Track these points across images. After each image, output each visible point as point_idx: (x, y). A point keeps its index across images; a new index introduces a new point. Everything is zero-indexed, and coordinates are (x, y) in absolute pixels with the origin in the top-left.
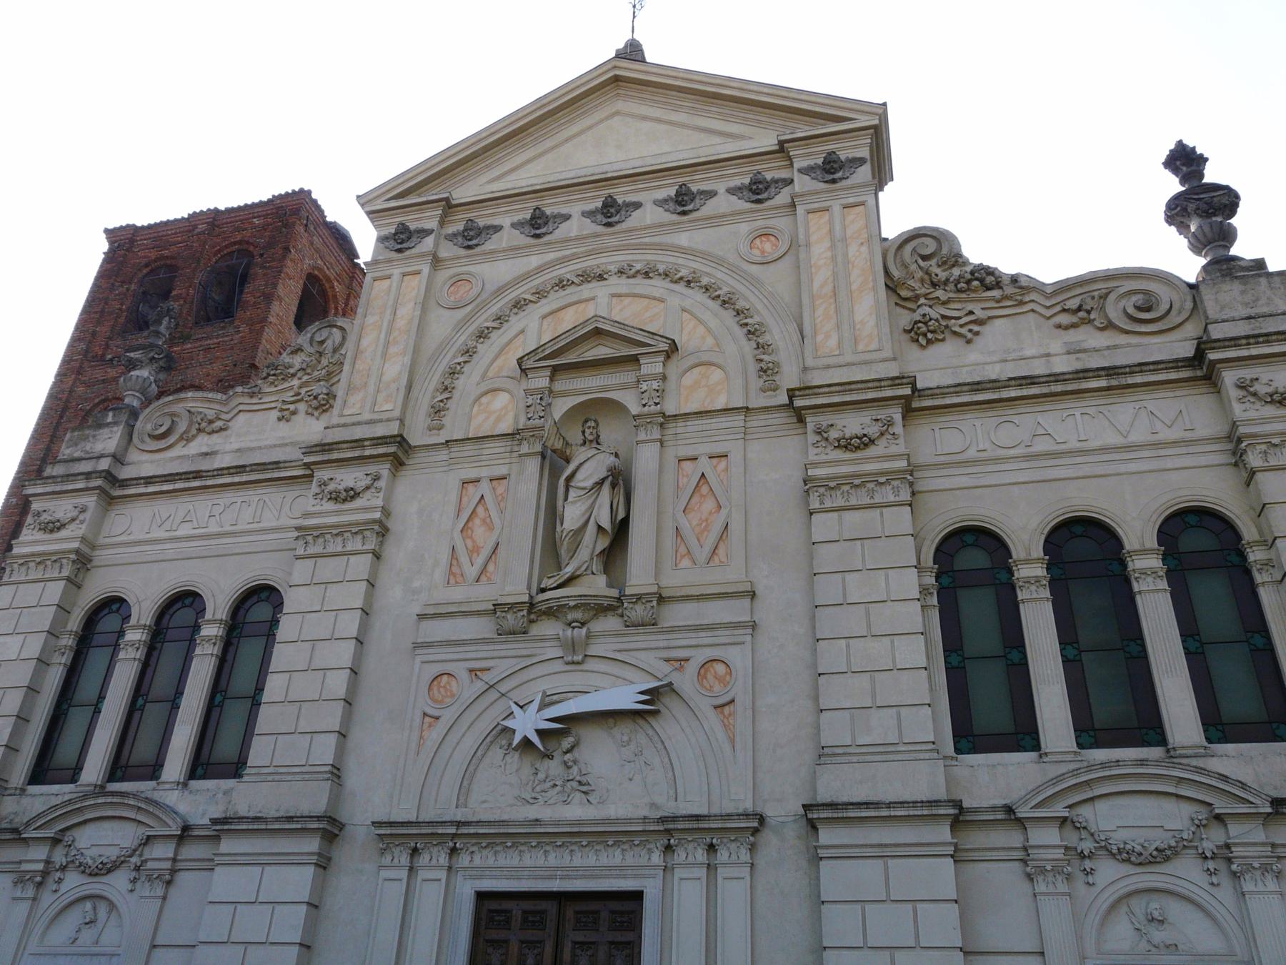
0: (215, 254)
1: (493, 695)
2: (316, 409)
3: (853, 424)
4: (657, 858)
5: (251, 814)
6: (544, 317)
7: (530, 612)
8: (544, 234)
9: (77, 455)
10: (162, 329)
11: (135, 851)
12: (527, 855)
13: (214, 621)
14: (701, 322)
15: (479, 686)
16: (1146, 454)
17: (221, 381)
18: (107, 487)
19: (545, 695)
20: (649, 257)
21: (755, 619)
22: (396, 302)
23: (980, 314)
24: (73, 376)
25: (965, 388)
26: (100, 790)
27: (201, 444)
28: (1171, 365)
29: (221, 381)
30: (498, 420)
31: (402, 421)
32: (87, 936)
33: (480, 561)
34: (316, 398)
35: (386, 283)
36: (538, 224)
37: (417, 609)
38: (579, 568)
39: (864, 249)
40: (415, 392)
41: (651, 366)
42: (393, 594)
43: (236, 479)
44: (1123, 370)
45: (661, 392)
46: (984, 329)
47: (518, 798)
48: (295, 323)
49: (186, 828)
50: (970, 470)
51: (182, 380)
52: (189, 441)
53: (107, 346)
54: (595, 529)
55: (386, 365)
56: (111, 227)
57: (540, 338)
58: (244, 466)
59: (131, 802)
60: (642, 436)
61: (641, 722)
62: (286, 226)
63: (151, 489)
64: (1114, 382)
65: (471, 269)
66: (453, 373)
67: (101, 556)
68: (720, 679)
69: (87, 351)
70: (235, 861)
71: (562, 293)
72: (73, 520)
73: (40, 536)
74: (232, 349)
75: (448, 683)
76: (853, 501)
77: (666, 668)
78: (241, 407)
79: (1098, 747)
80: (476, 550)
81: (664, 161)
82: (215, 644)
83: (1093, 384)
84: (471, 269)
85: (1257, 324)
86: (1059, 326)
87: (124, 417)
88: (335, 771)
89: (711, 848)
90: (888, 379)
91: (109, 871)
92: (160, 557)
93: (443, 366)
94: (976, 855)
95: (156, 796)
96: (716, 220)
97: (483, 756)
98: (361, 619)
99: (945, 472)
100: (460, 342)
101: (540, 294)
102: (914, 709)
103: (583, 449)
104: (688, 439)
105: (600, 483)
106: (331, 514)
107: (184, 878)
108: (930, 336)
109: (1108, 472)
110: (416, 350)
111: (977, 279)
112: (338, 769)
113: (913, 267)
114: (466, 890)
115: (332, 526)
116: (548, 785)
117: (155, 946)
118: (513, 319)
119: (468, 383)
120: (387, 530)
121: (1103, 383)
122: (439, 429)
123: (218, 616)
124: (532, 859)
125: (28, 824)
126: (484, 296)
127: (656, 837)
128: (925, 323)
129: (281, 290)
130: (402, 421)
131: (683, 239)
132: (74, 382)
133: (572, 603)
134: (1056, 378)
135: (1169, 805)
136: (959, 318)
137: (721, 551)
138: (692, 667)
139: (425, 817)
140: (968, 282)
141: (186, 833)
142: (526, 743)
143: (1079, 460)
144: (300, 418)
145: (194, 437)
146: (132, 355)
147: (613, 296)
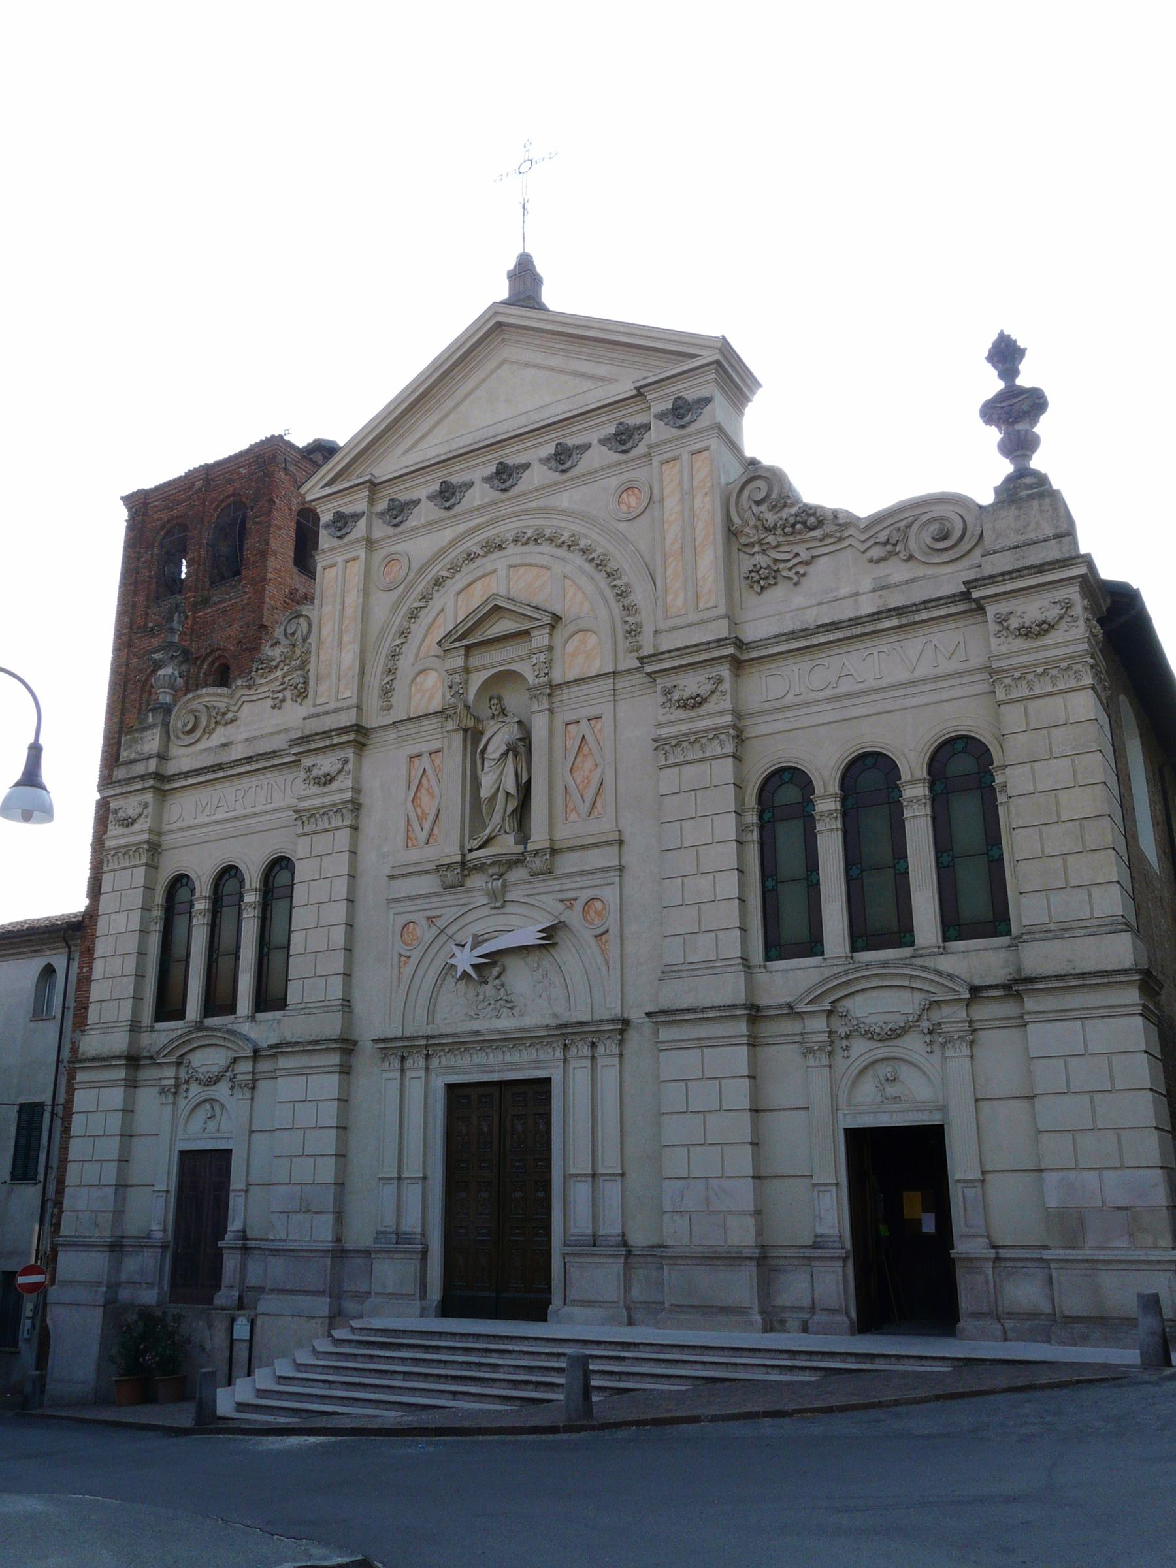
0: (215, 510)
1: (443, 938)
2: (298, 696)
3: (692, 684)
4: (559, 1054)
5: (294, 1040)
6: (459, 593)
7: (463, 869)
8: (454, 505)
9: (133, 756)
10: (175, 625)
11: (228, 1068)
12: (475, 1056)
13: (251, 890)
14: (579, 588)
15: (434, 931)
16: (928, 687)
17: (240, 642)
18: (158, 785)
19: (475, 936)
20: (537, 522)
21: (623, 863)
22: (343, 591)
23: (805, 556)
24: (126, 650)
25: (783, 638)
26: (200, 1026)
27: (220, 735)
28: (950, 600)
29: (240, 642)
30: (431, 697)
31: (359, 707)
32: (211, 1125)
33: (427, 825)
34: (296, 688)
35: (334, 571)
36: (447, 494)
37: (387, 871)
38: (493, 831)
39: (707, 499)
40: (367, 677)
41: (540, 639)
42: (369, 859)
43: (248, 768)
44: (910, 609)
45: (549, 663)
46: (811, 569)
47: (466, 1014)
48: (296, 564)
49: (256, 1051)
50: (788, 714)
51: (210, 645)
52: (211, 733)
53: (147, 614)
54: (504, 794)
55: (343, 655)
56: (125, 494)
57: (456, 615)
58: (250, 757)
59: (219, 1034)
60: (535, 707)
61: (544, 951)
62: (266, 475)
63: (191, 781)
64: (904, 621)
65: (399, 548)
66: (394, 655)
67: (168, 840)
68: (599, 914)
69: (132, 623)
70: (288, 1073)
71: (472, 566)
72: (140, 815)
73: (121, 831)
74: (243, 609)
75: (414, 929)
76: (690, 757)
77: (561, 907)
78: (244, 699)
79: (868, 950)
80: (421, 819)
81: (547, 415)
82: (255, 908)
83: (887, 624)
84: (399, 548)
85: (1022, 554)
86: (871, 561)
87: (160, 717)
88: (346, 1003)
89: (593, 1045)
90: (714, 641)
91: (215, 1083)
92: (207, 839)
93: (385, 651)
94: (770, 1041)
95: (236, 1027)
96: (591, 476)
97: (441, 984)
98: (348, 884)
99: (768, 718)
100: (397, 623)
101: (455, 569)
102: (728, 931)
103: (492, 722)
104: (573, 705)
105: (506, 754)
106: (318, 798)
107: (262, 1085)
108: (762, 583)
109: (896, 708)
110: (364, 636)
111: (799, 522)
112: (349, 1001)
113: (748, 514)
114: (438, 1084)
115: (319, 808)
116: (486, 1003)
117: (253, 1132)
118: (436, 595)
119: (405, 664)
120: (360, 805)
121: (894, 622)
122: (388, 710)
123: (254, 886)
124: (479, 1059)
125: (158, 1053)
126: (412, 575)
127: (557, 1038)
128: (757, 572)
129: (274, 544)
130: (359, 707)
131: (564, 500)
132: (128, 655)
133: (489, 862)
134: (856, 621)
135: (907, 995)
136: (789, 560)
137: (598, 804)
138: (579, 905)
139: (408, 1033)
140: (793, 526)
141: (256, 1054)
142: (465, 974)
143: (873, 697)
144: (288, 704)
145: (214, 729)
146: (156, 656)
147: (511, 566)
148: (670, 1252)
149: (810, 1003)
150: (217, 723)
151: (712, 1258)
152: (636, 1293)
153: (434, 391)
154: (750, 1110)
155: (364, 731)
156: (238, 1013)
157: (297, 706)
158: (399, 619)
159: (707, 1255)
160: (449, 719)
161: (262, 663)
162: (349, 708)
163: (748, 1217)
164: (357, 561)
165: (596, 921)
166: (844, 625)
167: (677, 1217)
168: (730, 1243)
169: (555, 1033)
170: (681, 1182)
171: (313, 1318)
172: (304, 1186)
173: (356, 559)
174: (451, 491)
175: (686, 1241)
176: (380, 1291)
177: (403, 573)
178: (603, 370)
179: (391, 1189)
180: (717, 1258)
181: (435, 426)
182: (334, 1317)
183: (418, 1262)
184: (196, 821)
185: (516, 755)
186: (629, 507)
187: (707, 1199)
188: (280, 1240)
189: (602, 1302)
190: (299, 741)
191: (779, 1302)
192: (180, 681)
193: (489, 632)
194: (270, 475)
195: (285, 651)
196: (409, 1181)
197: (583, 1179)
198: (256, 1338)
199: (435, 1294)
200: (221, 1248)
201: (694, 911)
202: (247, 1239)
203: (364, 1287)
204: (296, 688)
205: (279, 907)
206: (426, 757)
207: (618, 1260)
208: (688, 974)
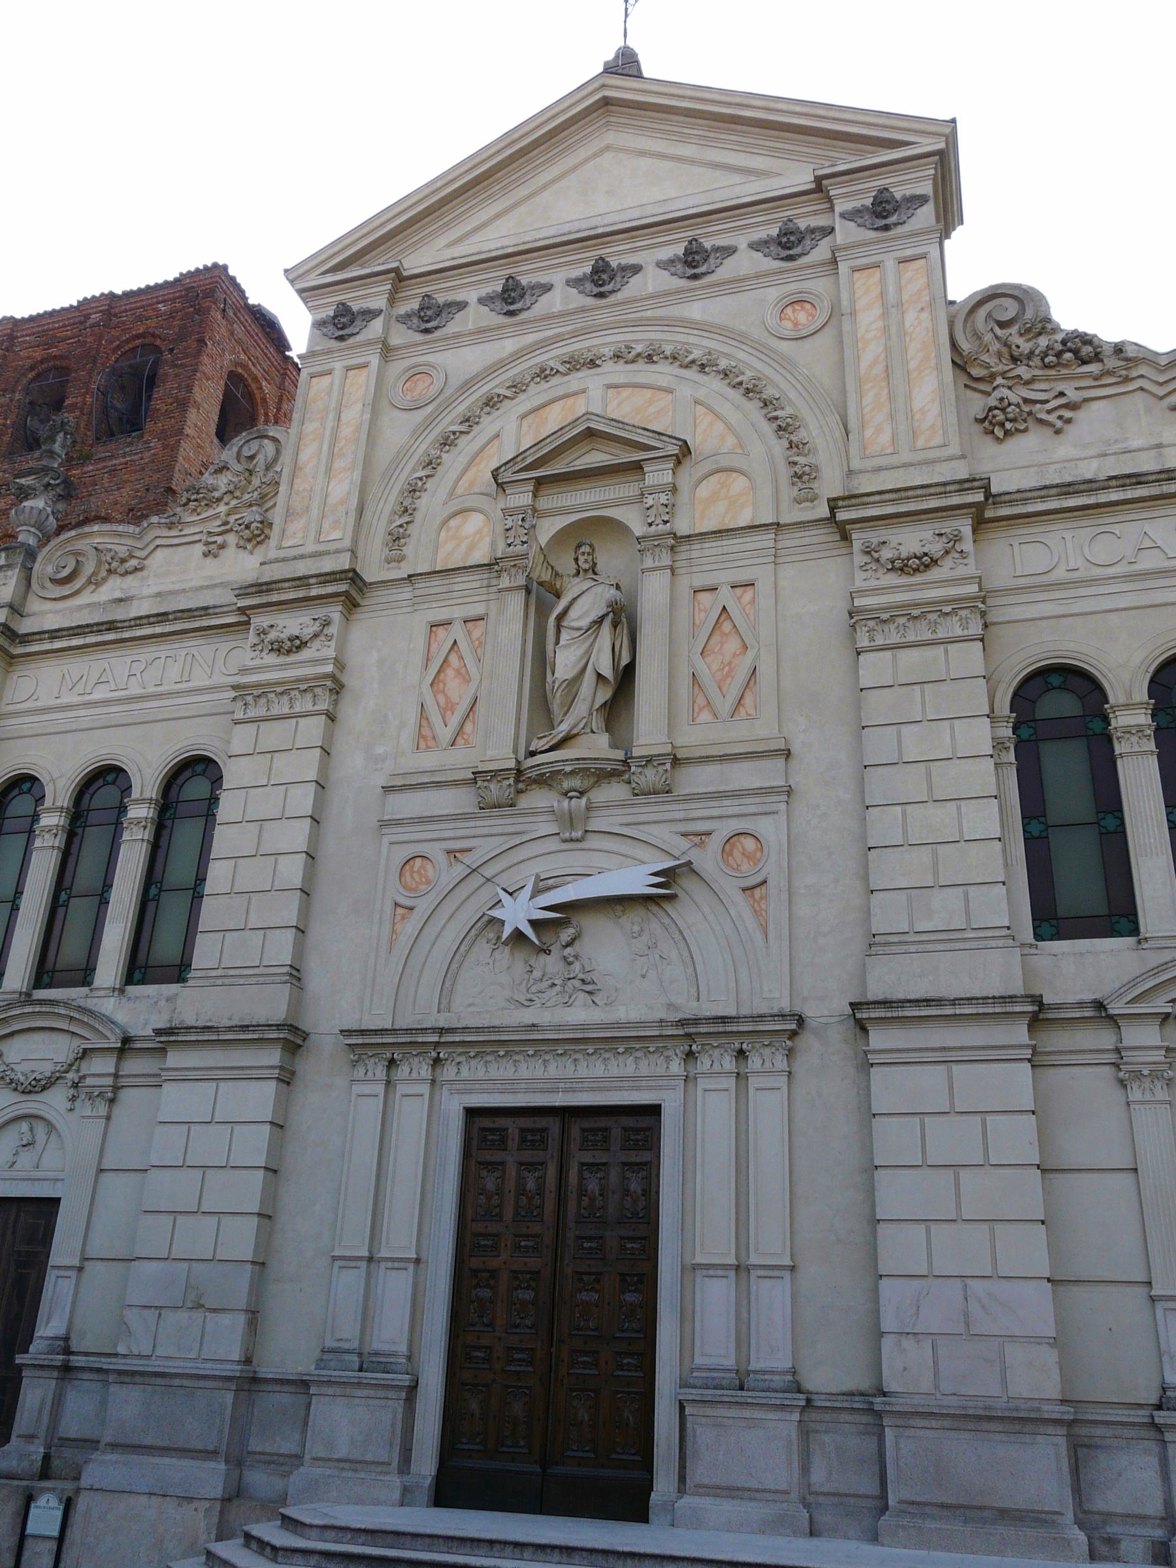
0: (114, 351)
1: (477, 880)
2: (249, 540)
4: (676, 1067)
5: (200, 1023)
6: (524, 416)
7: (517, 781)
8: (520, 310)
10: (57, 447)
11: (71, 1065)
12: (523, 1066)
14: (718, 416)
15: (459, 870)
17: (131, 510)
20: (652, 336)
21: (791, 783)
23: (1073, 395)
25: (1054, 491)
26: (26, 998)
27: (113, 588)
30: (472, 547)
31: (353, 552)
32: (26, 1159)
33: (454, 720)
34: (248, 527)
35: (326, 380)
38: (576, 726)
39: (925, 315)
40: (368, 514)
43: (158, 630)
46: (1080, 416)
47: (510, 1000)
48: (217, 434)
49: (126, 1040)
51: (85, 511)
52: (98, 585)
54: (594, 677)
55: (332, 484)
58: (166, 614)
59: (62, 1011)
61: (655, 908)
62: (198, 311)
63: (58, 644)
65: (430, 358)
66: (413, 490)
70: (184, 1077)
71: (544, 385)
74: (143, 469)
76: (911, 637)
77: (684, 844)
78: (158, 542)
82: (145, 827)
84: (430, 358)
89: (741, 1054)
95: (90, 1004)
96: (737, 284)
97: (468, 952)
100: (421, 451)
101: (518, 387)
102: (984, 888)
105: (599, 621)
107: (126, 1096)
108: (1008, 425)
110: (367, 464)
111: (1070, 350)
113: (988, 337)
114: (453, 1107)
116: (546, 984)
118: (485, 420)
119: (431, 503)
120: (342, 686)
122: (399, 562)
123: (147, 795)
124: (529, 1069)
126: (448, 392)
128: (1003, 410)
129: (198, 394)
130: (353, 552)
131: (695, 311)
136: (1047, 401)
137: (748, 701)
138: (715, 843)
140: (1059, 355)
141: (126, 1046)
142: (518, 935)
144: (230, 552)
145: (104, 580)
146: (22, 481)
147: (609, 386)
148: (899, 1404)
149: (1134, 1000)
150: (110, 571)
151: (979, 1418)
152: (818, 1476)
153: (500, 174)
154: (246, 1311)
155: (361, 584)
156: (97, 982)
157: (243, 555)
158: (424, 446)
159: (971, 1412)
160: (505, 574)
161: (198, 493)
162: (337, 552)
163: (1045, 1348)
164: (366, 369)
165: (745, 867)
166: (1151, 478)
167: (908, 1343)
168: (1014, 1391)
169: (675, 1032)
170: (915, 1283)
171: (190, 1499)
172: (194, 1264)
173: (364, 366)
174: (519, 291)
175: (926, 1385)
176: (322, 1455)
177: (434, 390)
178: (759, 162)
179: (350, 1280)
180: (990, 1419)
181: (498, 216)
182: (229, 1500)
183: (399, 1407)
184: (58, 701)
185: (615, 625)
186: (796, 324)
187: (966, 1314)
188: (140, 1356)
189: (758, 1491)
190: (254, 589)
191: (1099, 1504)
192: (52, 523)
193: (577, 463)
194: (202, 311)
195: (235, 479)
196: (390, 1265)
197: (720, 1273)
198: (74, 1534)
199: (426, 1465)
200: (20, 1368)
201: (925, 854)
202: (73, 1353)
203: (288, 1446)
204: (248, 527)
205: (186, 834)
206: (457, 627)
207: (787, 1416)
208: (920, 947)
